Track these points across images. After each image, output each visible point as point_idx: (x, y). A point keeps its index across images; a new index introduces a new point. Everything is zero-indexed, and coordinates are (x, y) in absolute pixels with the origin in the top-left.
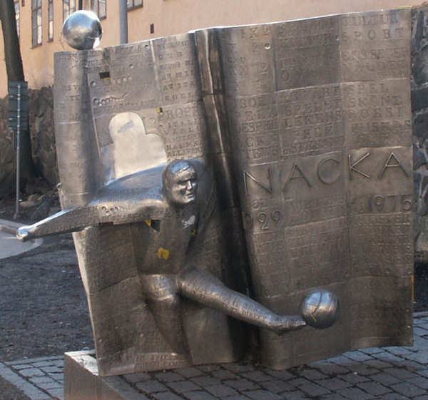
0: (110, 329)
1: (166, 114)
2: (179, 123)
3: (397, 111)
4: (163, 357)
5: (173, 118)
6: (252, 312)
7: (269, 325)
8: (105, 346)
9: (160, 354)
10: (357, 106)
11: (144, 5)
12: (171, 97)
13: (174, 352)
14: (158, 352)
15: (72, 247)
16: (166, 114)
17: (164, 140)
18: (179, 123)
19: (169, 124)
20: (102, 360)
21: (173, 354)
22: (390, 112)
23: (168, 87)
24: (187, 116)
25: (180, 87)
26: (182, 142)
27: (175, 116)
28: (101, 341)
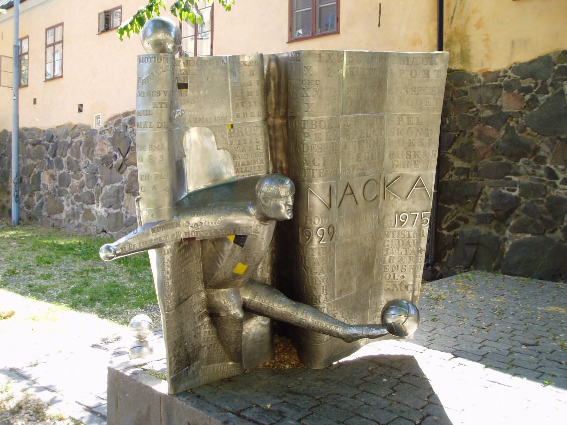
0: (180, 347)
1: (236, 131)
2: (248, 141)
3: (428, 141)
4: (222, 367)
5: (242, 135)
6: (82, 298)
7: (341, 334)
8: (176, 364)
9: (220, 364)
10: (396, 135)
11: (29, 85)
12: (241, 115)
13: (231, 361)
14: (218, 363)
15: (148, 264)
16: (236, 131)
17: (234, 157)
18: (248, 141)
19: (239, 141)
20: (172, 378)
21: (231, 363)
22: (422, 142)
23: (240, 105)
24: (255, 134)
25: (250, 106)
26: (250, 159)
27: (244, 134)
28: (173, 358)
